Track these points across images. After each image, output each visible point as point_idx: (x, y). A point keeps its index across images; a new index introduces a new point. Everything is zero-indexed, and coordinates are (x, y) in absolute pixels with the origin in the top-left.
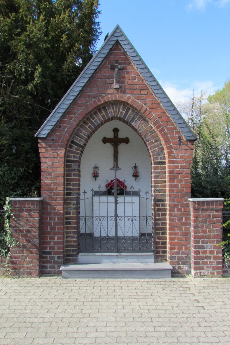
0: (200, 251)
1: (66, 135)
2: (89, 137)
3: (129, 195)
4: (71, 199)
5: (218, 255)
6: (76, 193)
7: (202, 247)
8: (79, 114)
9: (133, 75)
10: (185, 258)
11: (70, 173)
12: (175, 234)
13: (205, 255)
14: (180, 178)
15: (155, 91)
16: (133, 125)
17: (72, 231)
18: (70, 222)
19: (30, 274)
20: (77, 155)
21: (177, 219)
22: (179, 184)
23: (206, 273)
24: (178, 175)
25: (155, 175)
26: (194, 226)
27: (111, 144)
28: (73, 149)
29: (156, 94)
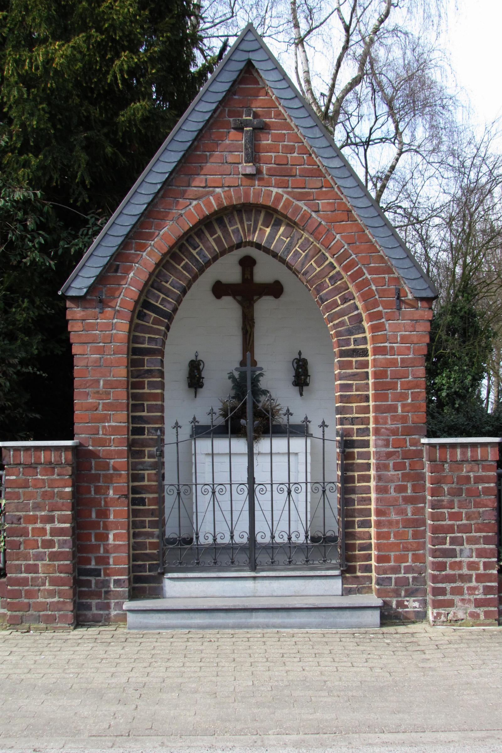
0: (446, 562)
1: (132, 290)
2: (184, 292)
3: (284, 435)
4: (145, 444)
5: (487, 572)
6: (156, 429)
7: (452, 553)
8: (162, 239)
9: (288, 142)
10: (413, 581)
11: (141, 380)
12: (390, 523)
13: (457, 572)
14: (401, 389)
15: (340, 182)
16: (289, 261)
17: (147, 519)
18: (143, 499)
19: (49, 620)
20: (157, 337)
21: (394, 488)
22: (399, 404)
23: (461, 615)
24: (397, 383)
25: (342, 382)
26: (432, 503)
27: (235, 298)
28: (148, 323)
29: (342, 189)
